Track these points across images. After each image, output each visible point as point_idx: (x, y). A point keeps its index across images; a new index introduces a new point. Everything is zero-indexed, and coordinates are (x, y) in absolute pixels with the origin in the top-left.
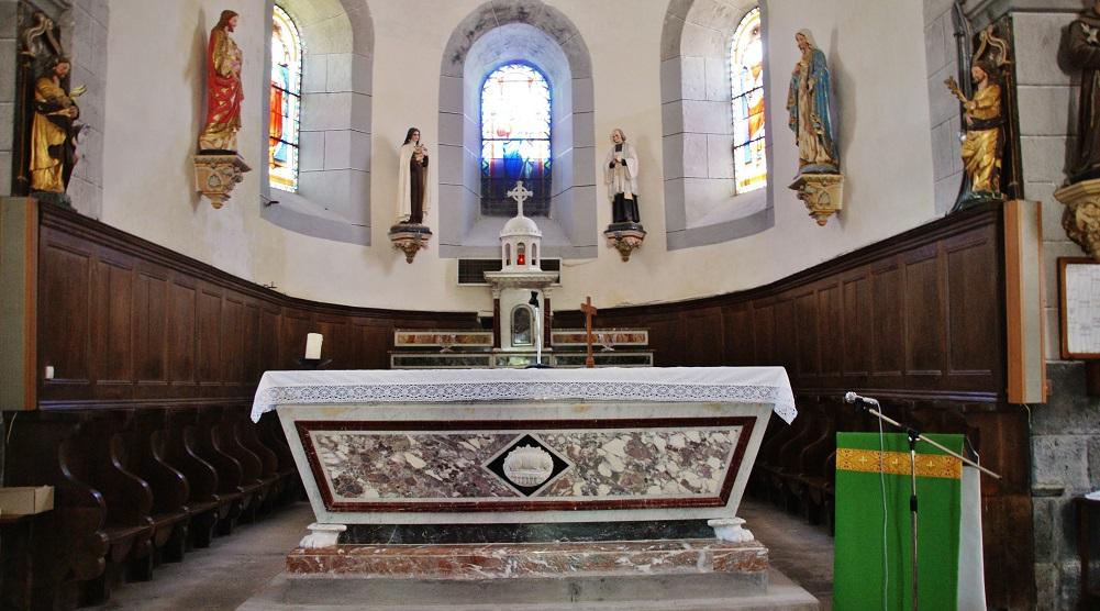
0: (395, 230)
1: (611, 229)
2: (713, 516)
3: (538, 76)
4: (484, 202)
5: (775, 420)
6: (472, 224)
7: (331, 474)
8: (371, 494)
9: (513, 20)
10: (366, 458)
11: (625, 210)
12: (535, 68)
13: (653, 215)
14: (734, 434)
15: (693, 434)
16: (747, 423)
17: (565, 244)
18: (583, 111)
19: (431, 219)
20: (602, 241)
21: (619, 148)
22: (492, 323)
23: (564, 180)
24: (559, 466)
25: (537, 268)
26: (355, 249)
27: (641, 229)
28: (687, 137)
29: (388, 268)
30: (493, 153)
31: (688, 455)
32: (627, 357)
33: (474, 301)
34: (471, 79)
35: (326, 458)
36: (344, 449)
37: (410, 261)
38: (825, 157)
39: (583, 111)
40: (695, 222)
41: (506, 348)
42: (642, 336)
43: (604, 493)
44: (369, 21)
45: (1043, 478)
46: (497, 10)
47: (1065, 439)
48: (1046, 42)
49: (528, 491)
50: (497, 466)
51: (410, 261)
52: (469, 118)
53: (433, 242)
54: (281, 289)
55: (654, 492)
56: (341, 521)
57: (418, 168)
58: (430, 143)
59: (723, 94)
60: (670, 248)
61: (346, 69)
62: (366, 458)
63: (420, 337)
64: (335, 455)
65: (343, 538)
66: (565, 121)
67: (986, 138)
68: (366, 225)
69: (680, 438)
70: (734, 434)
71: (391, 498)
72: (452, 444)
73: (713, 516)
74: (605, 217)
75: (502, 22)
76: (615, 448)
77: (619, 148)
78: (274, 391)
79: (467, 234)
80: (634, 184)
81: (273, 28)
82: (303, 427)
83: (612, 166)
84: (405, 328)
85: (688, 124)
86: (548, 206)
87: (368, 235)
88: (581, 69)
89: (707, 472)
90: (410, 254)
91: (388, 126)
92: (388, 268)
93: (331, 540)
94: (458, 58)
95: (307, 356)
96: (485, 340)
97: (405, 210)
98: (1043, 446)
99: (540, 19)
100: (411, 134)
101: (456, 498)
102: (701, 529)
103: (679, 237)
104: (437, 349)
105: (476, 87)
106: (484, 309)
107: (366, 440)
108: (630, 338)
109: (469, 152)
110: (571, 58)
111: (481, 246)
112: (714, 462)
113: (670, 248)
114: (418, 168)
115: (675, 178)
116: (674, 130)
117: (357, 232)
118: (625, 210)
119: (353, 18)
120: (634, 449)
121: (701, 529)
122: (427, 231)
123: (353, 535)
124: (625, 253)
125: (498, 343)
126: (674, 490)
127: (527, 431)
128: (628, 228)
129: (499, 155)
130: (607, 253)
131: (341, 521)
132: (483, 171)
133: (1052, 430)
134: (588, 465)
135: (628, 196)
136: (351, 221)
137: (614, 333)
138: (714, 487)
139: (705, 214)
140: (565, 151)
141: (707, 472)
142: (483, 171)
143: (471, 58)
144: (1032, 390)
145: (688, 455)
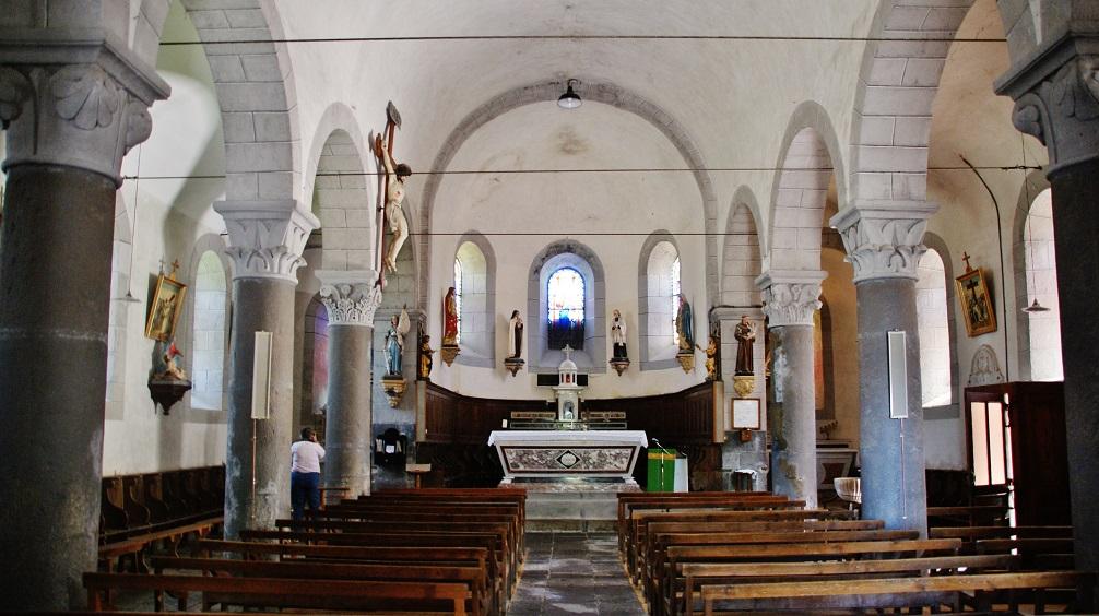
0: (507, 361)
1: (613, 360)
2: (624, 476)
3: (577, 275)
4: (550, 342)
5: (642, 447)
6: (544, 355)
7: (510, 462)
8: (522, 468)
9: (565, 251)
10: (521, 457)
11: (620, 352)
12: (576, 271)
13: (634, 354)
14: (630, 451)
15: (618, 451)
16: (634, 448)
17: (591, 366)
18: (600, 297)
19: (524, 355)
20: (609, 365)
21: (617, 320)
22: (554, 407)
23: (591, 330)
24: (578, 460)
25: (575, 384)
26: (488, 371)
27: (627, 360)
28: (650, 316)
29: (504, 379)
30: (554, 316)
31: (616, 457)
32: (615, 425)
33: (545, 394)
34: (543, 280)
35: (509, 456)
36: (514, 454)
37: (514, 375)
38: (688, 346)
39: (600, 297)
40: (652, 359)
41: (561, 419)
42: (623, 415)
43: (591, 468)
44: (494, 258)
45: (725, 466)
46: (556, 246)
47: (732, 454)
48: (731, 329)
49: (568, 452)
50: (559, 460)
51: (514, 375)
52: (542, 300)
53: (525, 366)
54: (461, 393)
55: (606, 468)
56: (513, 476)
57: (518, 331)
58: (523, 317)
59: (669, 293)
60: (641, 370)
61: (484, 283)
62: (521, 457)
63: (523, 414)
64: (511, 457)
65: (513, 481)
66: (591, 301)
67: (712, 360)
68: (493, 358)
69: (613, 452)
70: (630, 451)
71: (528, 469)
72: (546, 453)
73: (624, 476)
74: (610, 354)
75: (559, 252)
76: (594, 455)
77: (617, 320)
78: (495, 438)
79: (542, 359)
80: (624, 338)
81: (455, 263)
82: (502, 448)
83: (613, 328)
84: (516, 410)
85: (650, 308)
86: (582, 344)
87: (495, 363)
88: (599, 276)
89: (622, 462)
90: (514, 373)
91: (504, 309)
92: (504, 379)
93: (509, 482)
94: (537, 271)
95: (977, 484)
96: (552, 416)
97: (513, 352)
98: (725, 456)
99: (578, 250)
100: (515, 313)
101: (547, 469)
102: (621, 480)
103: (645, 365)
104: (530, 420)
105: (545, 287)
106: (550, 399)
107: (521, 451)
108: (618, 416)
109: (542, 317)
110: (594, 270)
111: (549, 367)
112: (624, 459)
113: (641, 370)
114: (518, 331)
115: (644, 336)
116: (644, 312)
117: (489, 362)
118: (620, 352)
119: (486, 257)
120: (600, 455)
121: (621, 480)
122: (523, 362)
123: (516, 480)
124: (620, 373)
125: (557, 418)
126: (612, 468)
127: (568, 449)
128: (620, 360)
129: (558, 318)
130: (611, 371)
131: (513, 476)
132: (549, 325)
133: (728, 451)
134: (586, 459)
135: (621, 344)
136: (487, 357)
137: (609, 413)
138: (624, 467)
139: (641, 366)
140: (591, 317)
141: (622, 462)
142: (549, 325)
143: (543, 270)
144: (720, 438)
145: (616, 457)
